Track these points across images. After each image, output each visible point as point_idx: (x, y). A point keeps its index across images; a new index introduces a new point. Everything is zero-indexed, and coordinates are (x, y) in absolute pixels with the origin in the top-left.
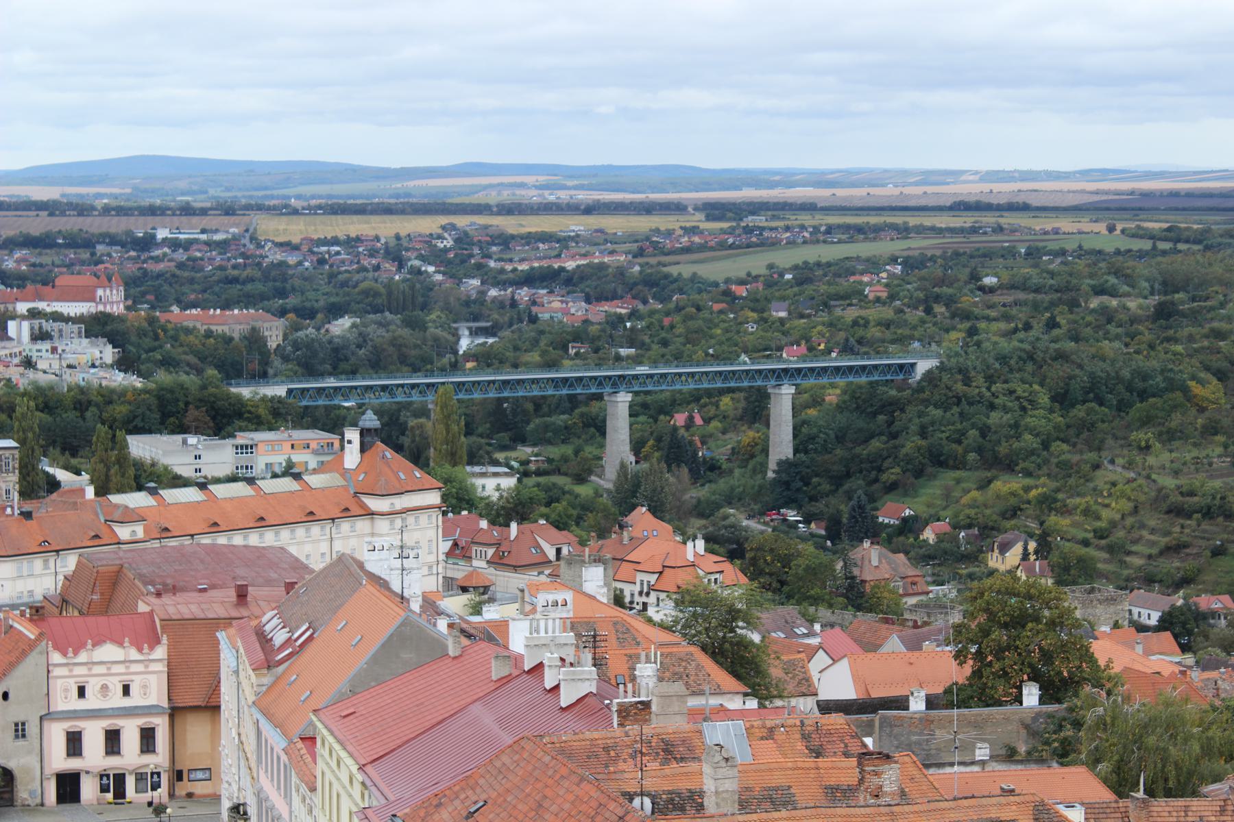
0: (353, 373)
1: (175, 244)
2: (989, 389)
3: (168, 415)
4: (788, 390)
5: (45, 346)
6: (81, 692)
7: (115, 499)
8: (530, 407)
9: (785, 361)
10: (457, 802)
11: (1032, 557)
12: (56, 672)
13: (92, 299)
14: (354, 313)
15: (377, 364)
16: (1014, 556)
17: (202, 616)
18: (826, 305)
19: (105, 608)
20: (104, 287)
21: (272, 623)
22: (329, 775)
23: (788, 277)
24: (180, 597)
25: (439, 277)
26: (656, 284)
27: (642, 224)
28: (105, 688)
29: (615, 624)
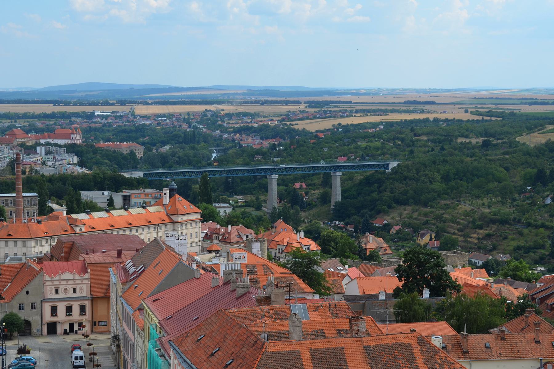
0: (170, 167)
1: (102, 117)
2: (417, 174)
3: (98, 184)
4: (339, 174)
5: (50, 156)
6: (57, 291)
7: (74, 216)
8: (238, 180)
9: (339, 163)
10: (193, 335)
11: (434, 240)
12: (47, 283)
13: (70, 139)
14: (172, 144)
15: (180, 162)
16: (426, 239)
17: (104, 262)
18: (354, 141)
19: (67, 258)
20: (74, 134)
21: (129, 264)
22: (148, 324)
23: (340, 130)
24: (96, 254)
25: (204, 130)
26: (291, 132)
27: (285, 108)
28: (66, 290)
29: (263, 265)
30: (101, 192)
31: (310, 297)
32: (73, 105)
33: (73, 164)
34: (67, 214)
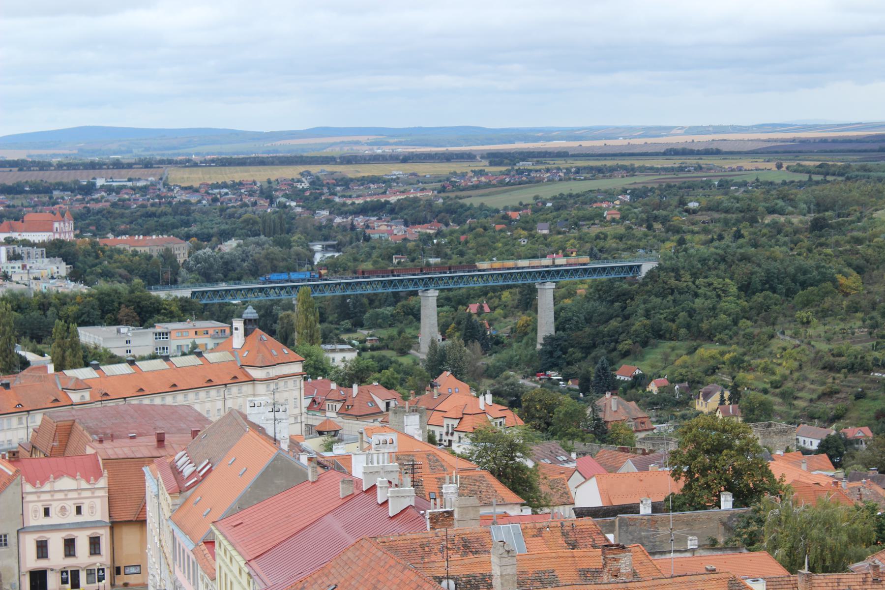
0: (239, 279)
1: (109, 190)
2: (694, 282)
3: (105, 312)
4: (550, 286)
5: (18, 264)
6: (47, 512)
7: (69, 373)
11: (727, 403)
12: (28, 498)
13: (51, 230)
17: (133, 456)
18: (576, 224)
21: (181, 460)
22: (224, 568)
23: (549, 205)
24: (117, 442)
25: (299, 210)
27: (444, 169)
28: (63, 509)
29: (428, 456)
30: (114, 328)
31: (514, 511)
32: (55, 170)
33: (61, 278)
34: (56, 370)
